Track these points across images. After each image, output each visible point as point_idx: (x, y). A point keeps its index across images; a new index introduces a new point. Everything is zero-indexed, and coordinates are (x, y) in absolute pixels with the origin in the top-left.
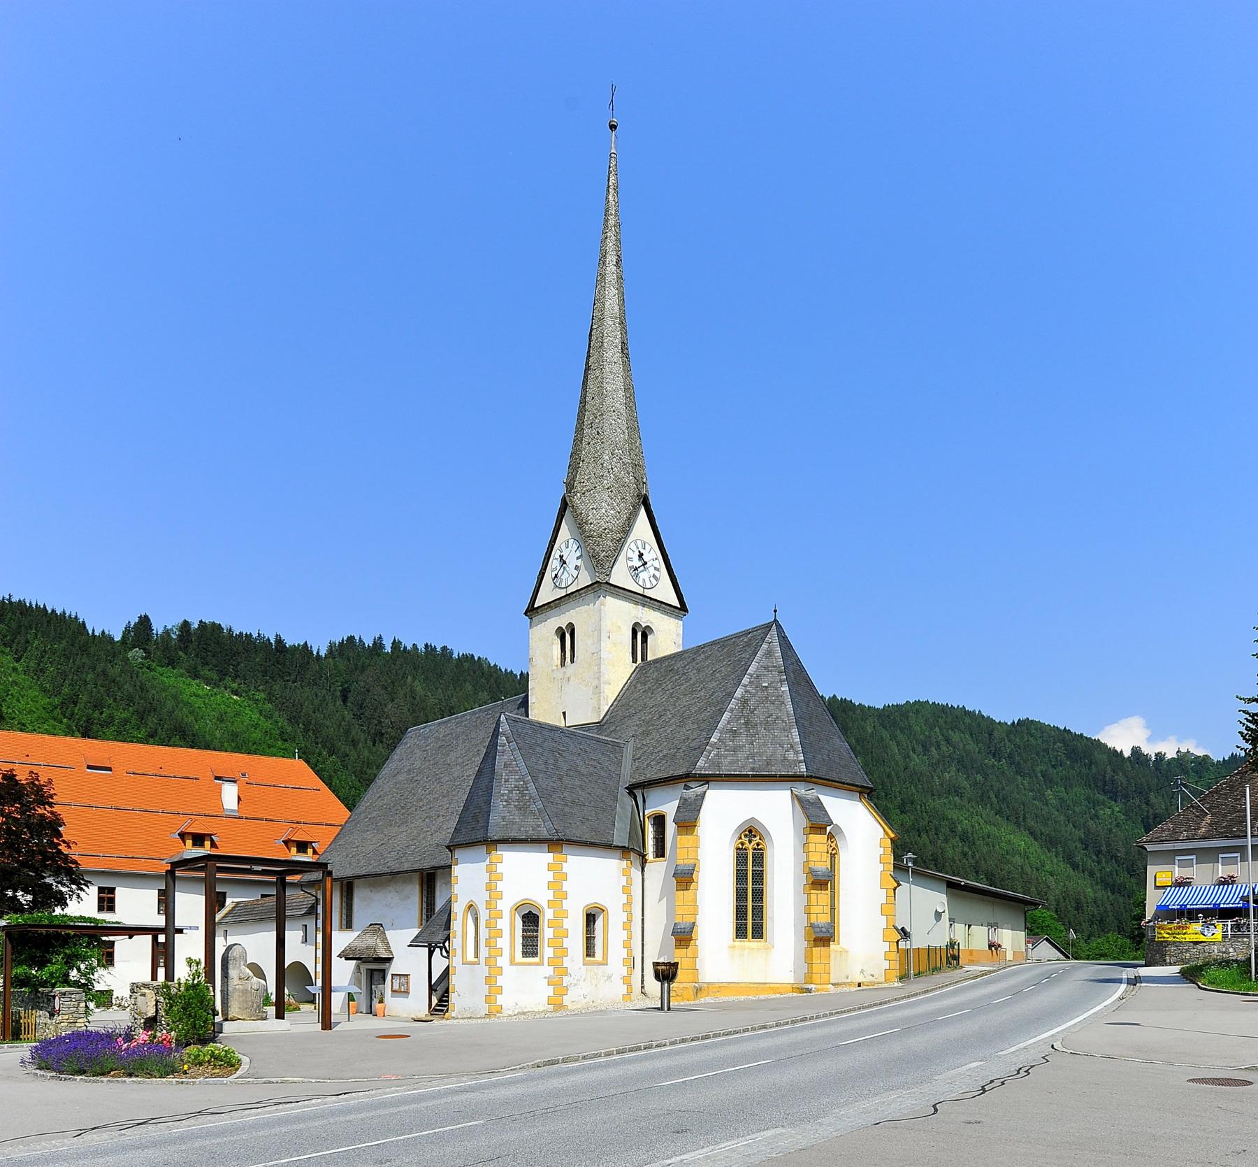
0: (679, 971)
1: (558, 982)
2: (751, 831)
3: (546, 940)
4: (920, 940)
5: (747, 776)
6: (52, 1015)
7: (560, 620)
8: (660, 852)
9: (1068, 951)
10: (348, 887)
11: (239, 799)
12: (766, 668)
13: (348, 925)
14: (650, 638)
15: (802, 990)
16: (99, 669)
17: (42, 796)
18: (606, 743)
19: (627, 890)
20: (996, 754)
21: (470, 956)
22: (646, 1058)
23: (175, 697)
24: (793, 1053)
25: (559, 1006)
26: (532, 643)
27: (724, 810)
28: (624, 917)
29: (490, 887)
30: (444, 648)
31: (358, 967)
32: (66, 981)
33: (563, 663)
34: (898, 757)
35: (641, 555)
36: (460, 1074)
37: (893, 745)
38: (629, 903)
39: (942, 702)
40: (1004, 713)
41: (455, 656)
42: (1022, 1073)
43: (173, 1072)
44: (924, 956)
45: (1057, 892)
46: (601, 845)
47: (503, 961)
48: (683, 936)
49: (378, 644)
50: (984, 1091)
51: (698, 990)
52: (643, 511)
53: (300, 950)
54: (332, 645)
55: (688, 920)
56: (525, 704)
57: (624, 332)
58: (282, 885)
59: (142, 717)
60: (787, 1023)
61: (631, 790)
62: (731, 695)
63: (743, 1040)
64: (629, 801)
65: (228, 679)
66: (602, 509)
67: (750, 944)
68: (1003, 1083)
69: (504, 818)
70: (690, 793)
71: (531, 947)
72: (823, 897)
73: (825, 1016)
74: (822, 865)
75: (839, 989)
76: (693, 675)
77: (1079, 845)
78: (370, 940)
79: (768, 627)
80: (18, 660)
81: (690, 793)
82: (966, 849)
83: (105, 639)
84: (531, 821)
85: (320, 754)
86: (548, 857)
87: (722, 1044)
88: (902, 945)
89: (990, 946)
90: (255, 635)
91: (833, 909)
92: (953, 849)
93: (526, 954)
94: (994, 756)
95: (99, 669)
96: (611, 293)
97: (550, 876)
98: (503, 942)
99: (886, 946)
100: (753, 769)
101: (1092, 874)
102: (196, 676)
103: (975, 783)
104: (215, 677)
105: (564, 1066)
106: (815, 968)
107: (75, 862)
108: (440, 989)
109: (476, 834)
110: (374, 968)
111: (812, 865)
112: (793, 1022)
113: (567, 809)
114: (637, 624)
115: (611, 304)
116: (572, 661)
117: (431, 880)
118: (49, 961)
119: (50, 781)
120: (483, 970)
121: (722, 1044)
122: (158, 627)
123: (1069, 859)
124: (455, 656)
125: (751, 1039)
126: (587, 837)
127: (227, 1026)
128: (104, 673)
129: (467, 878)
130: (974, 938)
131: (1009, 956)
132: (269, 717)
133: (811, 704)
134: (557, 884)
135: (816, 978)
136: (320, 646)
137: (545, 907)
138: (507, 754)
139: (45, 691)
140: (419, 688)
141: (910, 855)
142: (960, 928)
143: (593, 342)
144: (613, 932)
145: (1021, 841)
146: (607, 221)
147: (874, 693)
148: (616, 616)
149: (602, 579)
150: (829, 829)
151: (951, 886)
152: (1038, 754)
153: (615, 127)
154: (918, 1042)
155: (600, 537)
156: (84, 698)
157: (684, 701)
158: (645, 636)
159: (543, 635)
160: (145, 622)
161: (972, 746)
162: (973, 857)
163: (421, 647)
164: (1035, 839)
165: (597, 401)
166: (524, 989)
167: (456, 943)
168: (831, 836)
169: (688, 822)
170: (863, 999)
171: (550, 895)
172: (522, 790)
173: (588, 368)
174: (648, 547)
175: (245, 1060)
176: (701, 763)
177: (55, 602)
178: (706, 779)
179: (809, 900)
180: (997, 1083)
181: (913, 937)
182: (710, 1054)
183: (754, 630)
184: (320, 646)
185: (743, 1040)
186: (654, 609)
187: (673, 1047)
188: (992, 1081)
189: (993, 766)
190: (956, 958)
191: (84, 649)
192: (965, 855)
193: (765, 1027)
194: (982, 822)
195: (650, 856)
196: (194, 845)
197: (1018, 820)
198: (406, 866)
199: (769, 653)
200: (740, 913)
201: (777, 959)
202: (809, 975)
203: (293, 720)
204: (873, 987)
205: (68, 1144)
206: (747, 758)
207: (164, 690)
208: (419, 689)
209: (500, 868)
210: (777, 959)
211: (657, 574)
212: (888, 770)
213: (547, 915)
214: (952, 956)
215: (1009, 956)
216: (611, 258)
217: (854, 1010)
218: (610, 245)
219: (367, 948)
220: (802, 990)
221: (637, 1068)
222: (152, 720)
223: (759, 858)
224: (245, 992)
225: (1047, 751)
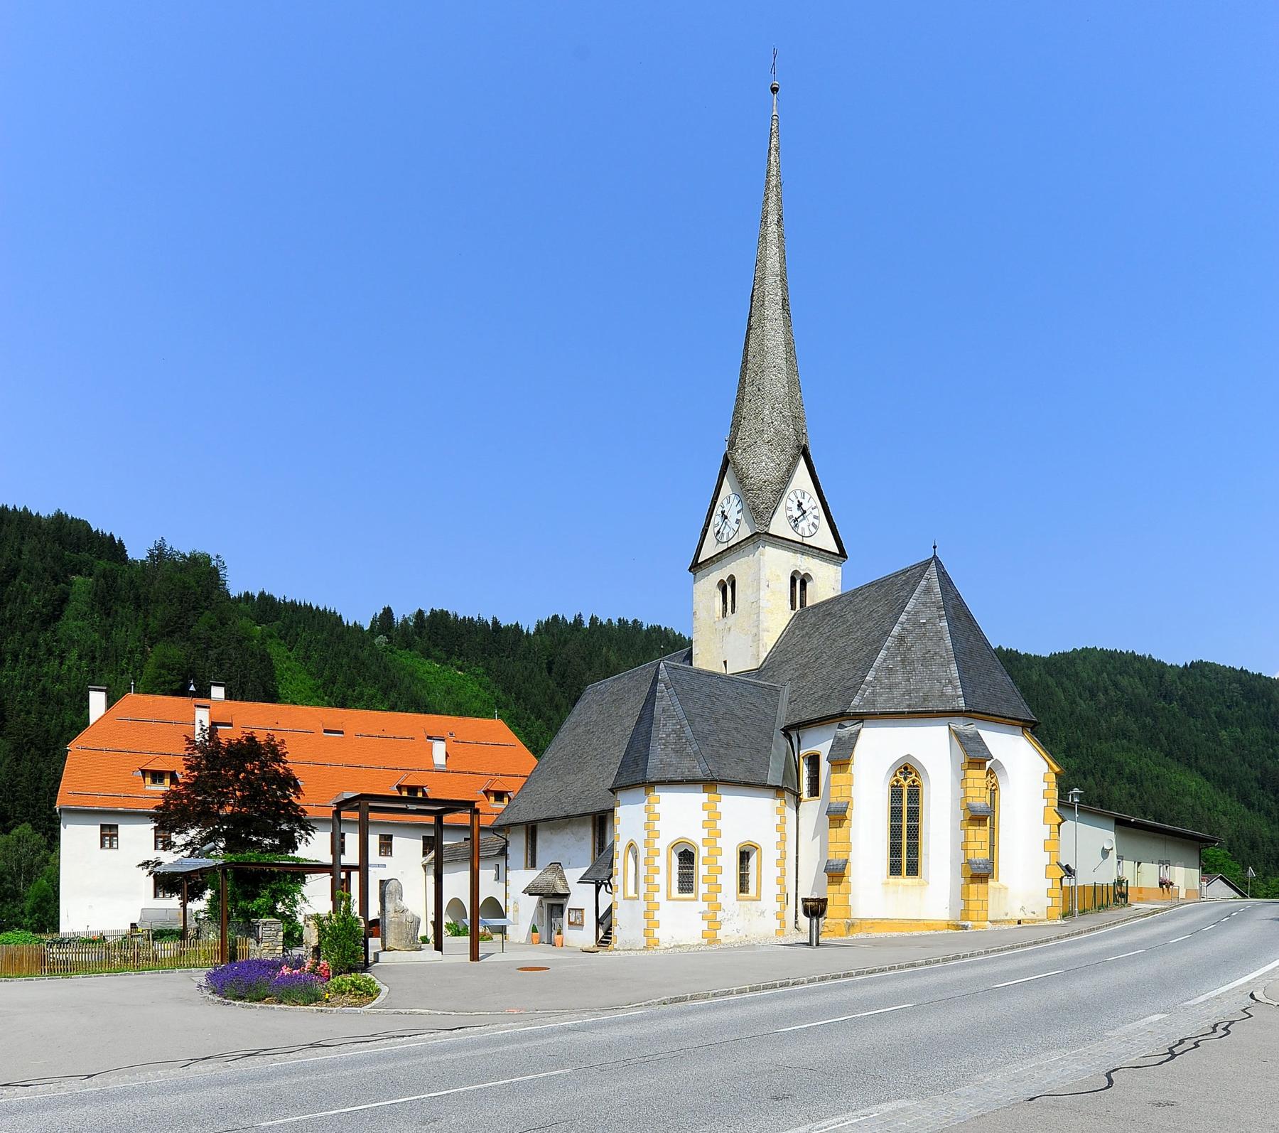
0: (828, 908)
1: (713, 920)
2: (906, 768)
3: (702, 876)
4: (1085, 878)
5: (903, 713)
7: (721, 574)
8: (814, 791)
9: (1243, 888)
10: (531, 830)
11: (447, 755)
12: (924, 604)
14: (808, 585)
15: (957, 927)
16: (352, 654)
17: (277, 754)
18: (763, 687)
19: (780, 828)
20: (1167, 697)
21: (631, 893)
22: (778, 997)
23: (411, 675)
24: (939, 996)
25: (713, 940)
26: (696, 598)
27: (879, 748)
28: (778, 855)
29: (649, 826)
30: (635, 621)
31: (540, 902)
33: (724, 615)
34: (1064, 703)
35: (800, 505)
36: (583, 1010)
37: (1059, 692)
38: (783, 841)
39: (1111, 648)
40: (1175, 654)
41: (645, 628)
42: (1220, 1032)
43: (316, 1000)
44: (1090, 894)
45: (1230, 831)
46: (756, 785)
47: (660, 897)
48: (836, 873)
49: (578, 621)
50: (1174, 1056)
51: (850, 926)
52: (802, 462)
53: (489, 887)
54: (539, 623)
55: (842, 856)
56: (689, 657)
57: (785, 288)
58: (440, 827)
59: (385, 693)
60: (938, 962)
61: (787, 731)
62: (887, 633)
63: (887, 979)
64: (784, 742)
65: (454, 657)
66: (761, 463)
67: (904, 880)
68: (1196, 1045)
69: (661, 760)
70: (844, 732)
71: (686, 883)
72: (982, 833)
73: (980, 954)
74: (979, 799)
75: (997, 927)
76: (850, 617)
77: (1255, 785)
79: (927, 564)
80: (290, 650)
81: (844, 732)
82: (1134, 791)
83: (357, 628)
84: (687, 763)
85: (529, 719)
86: (704, 797)
87: (864, 983)
88: (1066, 882)
89: (1161, 884)
90: (476, 619)
91: (992, 846)
92: (1119, 791)
93: (681, 890)
94: (1165, 698)
95: (352, 654)
96: (773, 251)
97: (704, 815)
98: (661, 879)
99: (1049, 883)
100: (909, 706)
101: (1268, 813)
102: (428, 656)
103: (1144, 726)
104: (444, 656)
105: (691, 1003)
106: (972, 905)
107: (303, 811)
108: (606, 926)
109: (636, 777)
110: (553, 903)
111: (970, 800)
112: (944, 960)
113: (722, 751)
114: (796, 572)
115: (773, 263)
116: (733, 612)
117: (601, 822)
118: (258, 895)
119: (283, 741)
120: (641, 906)
121: (864, 983)
122: (398, 617)
123: (1244, 798)
124: (645, 628)
125: (897, 977)
126: (741, 778)
127: (382, 956)
128: (356, 657)
129: (629, 818)
130: (1144, 875)
131: (1182, 894)
132: (487, 689)
133: (971, 638)
134: (711, 824)
135: (973, 915)
136: (529, 626)
137: (700, 844)
138: (666, 700)
139: (310, 673)
140: (613, 658)
141: (1076, 790)
142: (1128, 865)
143: (755, 300)
144: (766, 870)
145: (1192, 782)
146: (768, 182)
147: (1040, 642)
148: (775, 565)
149: (762, 529)
150: (988, 764)
151: (1121, 824)
152: (1211, 695)
153: (777, 89)
154: (1084, 987)
155: (760, 489)
156: (340, 678)
157: (840, 643)
158: (804, 584)
159: (706, 589)
160: (388, 612)
161: (1141, 690)
162: (1141, 798)
163: (615, 621)
164: (1208, 780)
165: (759, 358)
166: (680, 923)
167: (617, 880)
168: (990, 772)
169: (841, 761)
170: (1024, 937)
171: (704, 833)
172: (679, 734)
173: (750, 327)
174: (807, 496)
175: (385, 989)
176: (855, 702)
178: (861, 718)
179: (966, 836)
180: (1189, 1044)
181: (1078, 874)
182: (848, 994)
183: (913, 568)
184: (529, 626)
185: (887, 979)
186: (813, 556)
187: (811, 986)
188: (1181, 1042)
189: (1164, 708)
190: (1124, 895)
191: (340, 638)
192: (1132, 796)
193: (913, 966)
194: (1151, 763)
195: (805, 795)
197: (1190, 761)
198: (580, 810)
199: (928, 590)
200: (895, 850)
201: (933, 895)
202: (965, 913)
203: (507, 690)
204: (1034, 925)
205: (176, 1074)
206: (903, 695)
207: (403, 669)
208: (613, 658)
209: (658, 808)
210: (933, 895)
211: (816, 522)
212: (1053, 716)
213: (701, 853)
214: (1120, 893)
215: (1182, 894)
216: (773, 218)
217: (1013, 948)
218: (772, 206)
219: (548, 885)
220: (957, 927)
221: (765, 1008)
222: (393, 695)
223: (915, 795)
224: (400, 924)
225: (1221, 692)
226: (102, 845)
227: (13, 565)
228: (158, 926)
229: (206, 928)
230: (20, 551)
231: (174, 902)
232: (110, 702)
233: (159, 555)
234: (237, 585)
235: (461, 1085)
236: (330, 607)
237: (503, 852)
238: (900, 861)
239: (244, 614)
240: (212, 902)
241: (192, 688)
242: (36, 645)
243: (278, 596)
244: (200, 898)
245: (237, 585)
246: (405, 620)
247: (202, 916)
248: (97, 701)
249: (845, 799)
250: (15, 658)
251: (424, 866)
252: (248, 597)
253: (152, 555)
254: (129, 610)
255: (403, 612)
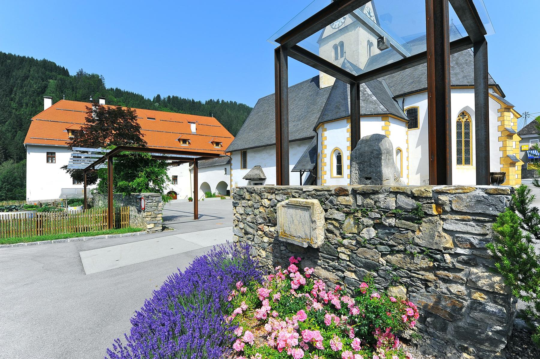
5: (467, 85)
6: (139, 211)
10: (244, 153)
13: (244, 166)
32: (147, 188)
49: (218, 101)
54: (206, 102)
78: (257, 172)
83: (149, 100)
86: (383, 123)
122: (162, 98)
160: (159, 96)
163: (229, 102)
177: (136, 92)
196: (183, 143)
206: (463, 78)
226: (48, 161)
227: (26, 75)
228: (71, 197)
229: (97, 198)
230: (30, 71)
231: (81, 186)
232: (53, 103)
233: (81, 74)
236: (140, 93)
237: (229, 162)
238: (461, 158)
240: (100, 185)
241: (91, 99)
242: (35, 101)
243: (122, 89)
244: (94, 183)
247: (95, 191)
248: (48, 103)
250: (27, 105)
251: (190, 170)
253: (78, 74)
254: (70, 91)
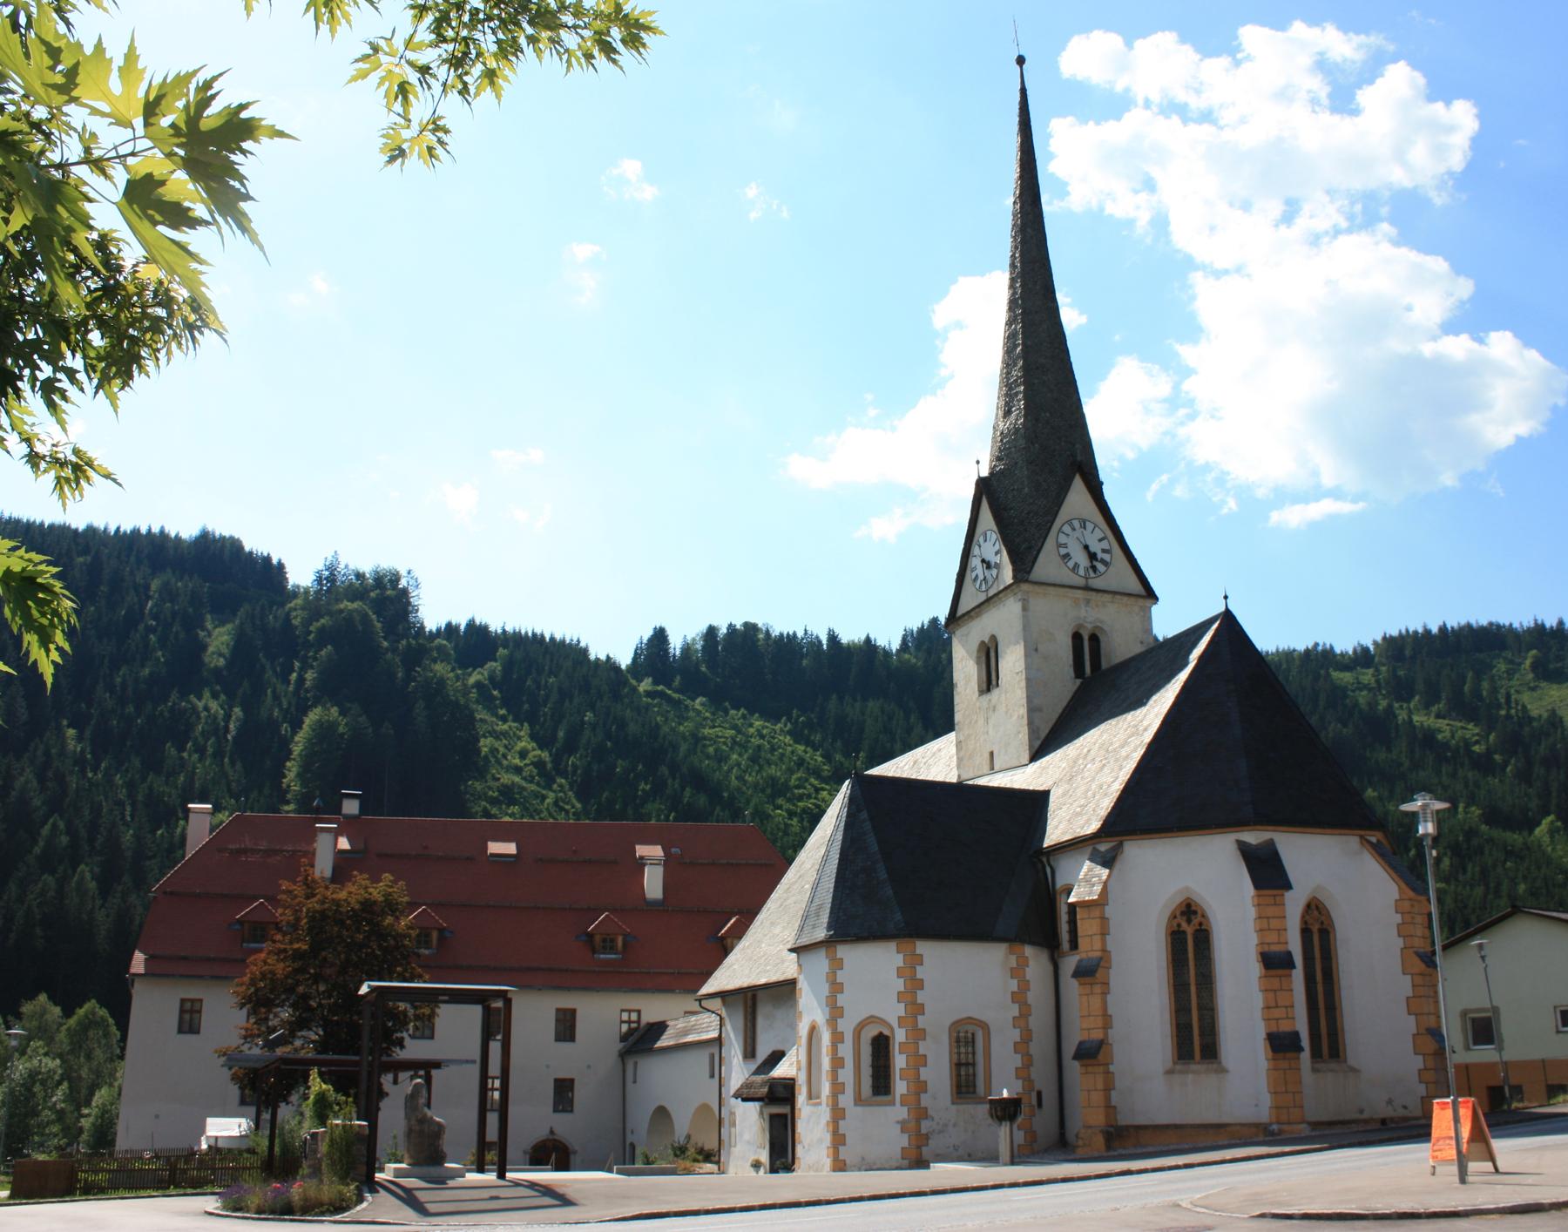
67: (563, 1074)
83: (610, 665)
90: (800, 634)
99: (1419, 1062)
122: (675, 644)
137: (895, 1024)
160: (660, 636)
195: (1066, 945)
233: (329, 579)
234: (433, 612)
235: (420, 978)
239: (443, 655)
243: (495, 626)
245: (433, 612)
246: (687, 649)
249: (1099, 954)
252: (451, 629)
253: (319, 580)
255: (683, 633)
